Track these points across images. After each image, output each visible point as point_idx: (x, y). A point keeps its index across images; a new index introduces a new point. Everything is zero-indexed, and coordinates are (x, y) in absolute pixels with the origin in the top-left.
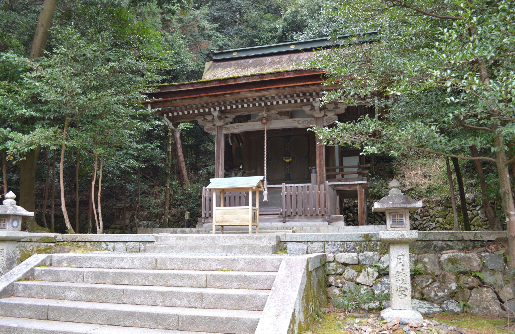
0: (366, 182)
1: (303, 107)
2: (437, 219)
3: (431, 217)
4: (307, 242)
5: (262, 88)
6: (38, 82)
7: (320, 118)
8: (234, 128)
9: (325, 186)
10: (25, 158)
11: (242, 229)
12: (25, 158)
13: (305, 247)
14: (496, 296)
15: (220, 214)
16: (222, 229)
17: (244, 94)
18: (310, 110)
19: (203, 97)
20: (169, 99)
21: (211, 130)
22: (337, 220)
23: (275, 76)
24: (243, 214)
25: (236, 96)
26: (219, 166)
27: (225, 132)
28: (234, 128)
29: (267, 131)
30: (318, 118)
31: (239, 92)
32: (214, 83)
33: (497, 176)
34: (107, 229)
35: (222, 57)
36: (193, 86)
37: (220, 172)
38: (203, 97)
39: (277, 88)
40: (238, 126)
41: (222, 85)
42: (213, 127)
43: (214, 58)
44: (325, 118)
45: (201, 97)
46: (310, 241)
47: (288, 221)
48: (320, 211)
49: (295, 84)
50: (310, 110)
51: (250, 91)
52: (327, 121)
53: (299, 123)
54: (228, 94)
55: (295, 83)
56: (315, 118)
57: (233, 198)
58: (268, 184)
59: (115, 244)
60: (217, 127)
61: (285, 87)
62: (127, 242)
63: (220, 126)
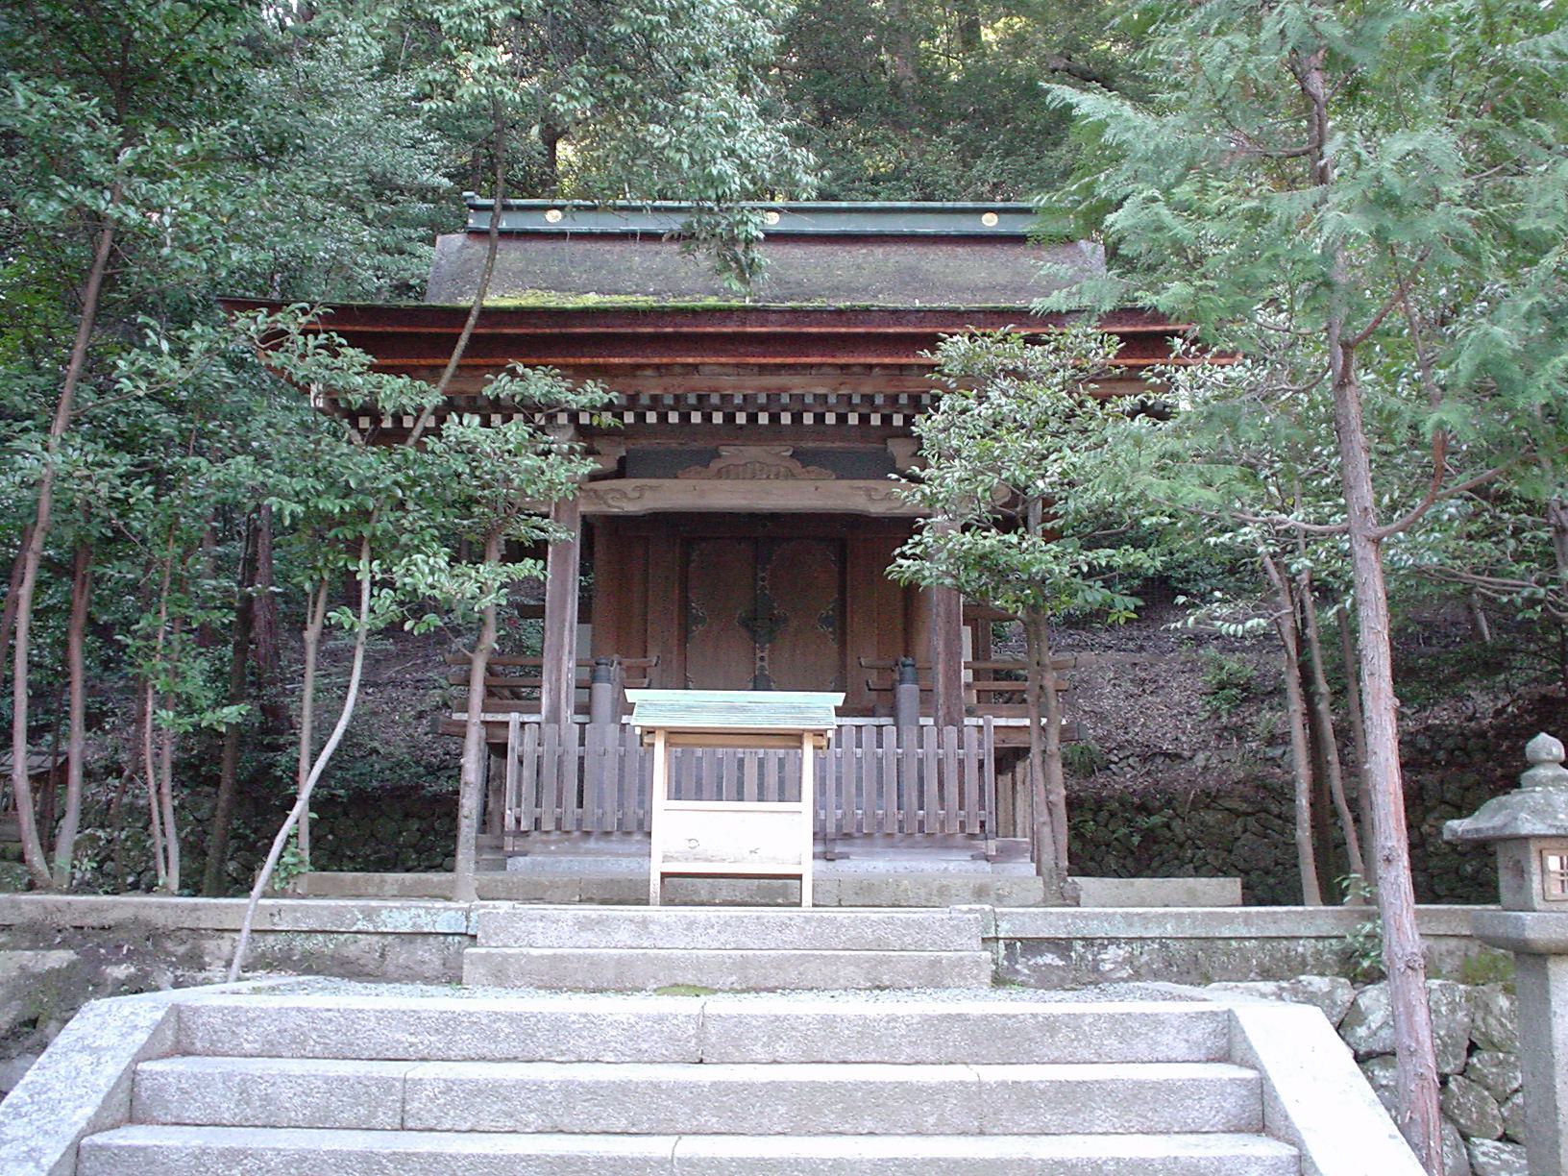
1: (890, 442)
2: (1200, 853)
3: (1181, 846)
5: (790, 360)
6: (541, 132)
8: (624, 495)
9: (960, 732)
11: (773, 889)
15: (686, 832)
16: (680, 888)
20: (415, 362)
24: (774, 835)
25: (677, 384)
26: (561, 634)
28: (624, 495)
33: (88, 707)
34: (192, 885)
40: (641, 489)
47: (845, 856)
48: (921, 823)
49: (852, 361)
53: (870, 498)
54: (649, 366)
57: (714, 769)
58: (485, 710)
61: (871, 367)
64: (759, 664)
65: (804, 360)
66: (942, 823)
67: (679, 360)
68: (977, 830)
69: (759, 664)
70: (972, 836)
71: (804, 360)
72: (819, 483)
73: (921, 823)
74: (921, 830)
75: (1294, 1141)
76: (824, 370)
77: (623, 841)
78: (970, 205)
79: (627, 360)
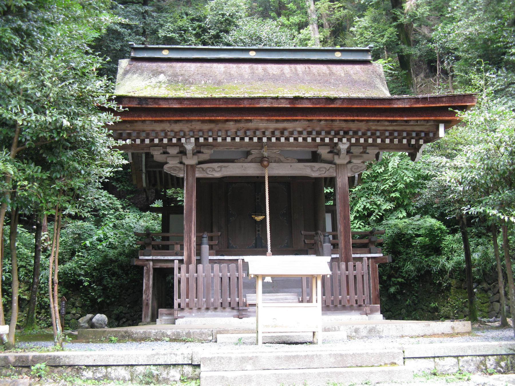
0: (381, 255)
4: (434, 357)
7: (344, 165)
8: (214, 170)
10: (26, 219)
12: (26, 219)
13: (429, 364)
14: (61, 364)
17: (259, 123)
18: (329, 152)
19: (191, 121)
21: (175, 170)
22: (372, 312)
23: (313, 103)
27: (198, 175)
28: (214, 170)
29: (269, 177)
30: (341, 165)
31: (251, 121)
32: (217, 102)
35: (146, 55)
36: (181, 103)
37: (193, 236)
38: (191, 121)
39: (309, 120)
40: (221, 167)
41: (230, 106)
42: (179, 165)
43: (133, 54)
44: (349, 166)
45: (188, 121)
46: (438, 357)
48: (340, 301)
50: (329, 152)
51: (267, 120)
52: (352, 171)
53: (312, 170)
55: (339, 115)
56: (335, 164)
59: (109, 369)
60: (187, 166)
62: (132, 365)
63: (192, 166)
64: (257, 233)
65: (295, 118)
66: (348, 301)
67: (245, 118)
68: (362, 304)
69: (257, 233)
70: (360, 306)
71: (295, 118)
72: (292, 164)
73: (340, 301)
74: (340, 303)
75: (2, 237)
76: (302, 121)
77: (222, 311)
78: (331, 48)
79: (224, 118)
